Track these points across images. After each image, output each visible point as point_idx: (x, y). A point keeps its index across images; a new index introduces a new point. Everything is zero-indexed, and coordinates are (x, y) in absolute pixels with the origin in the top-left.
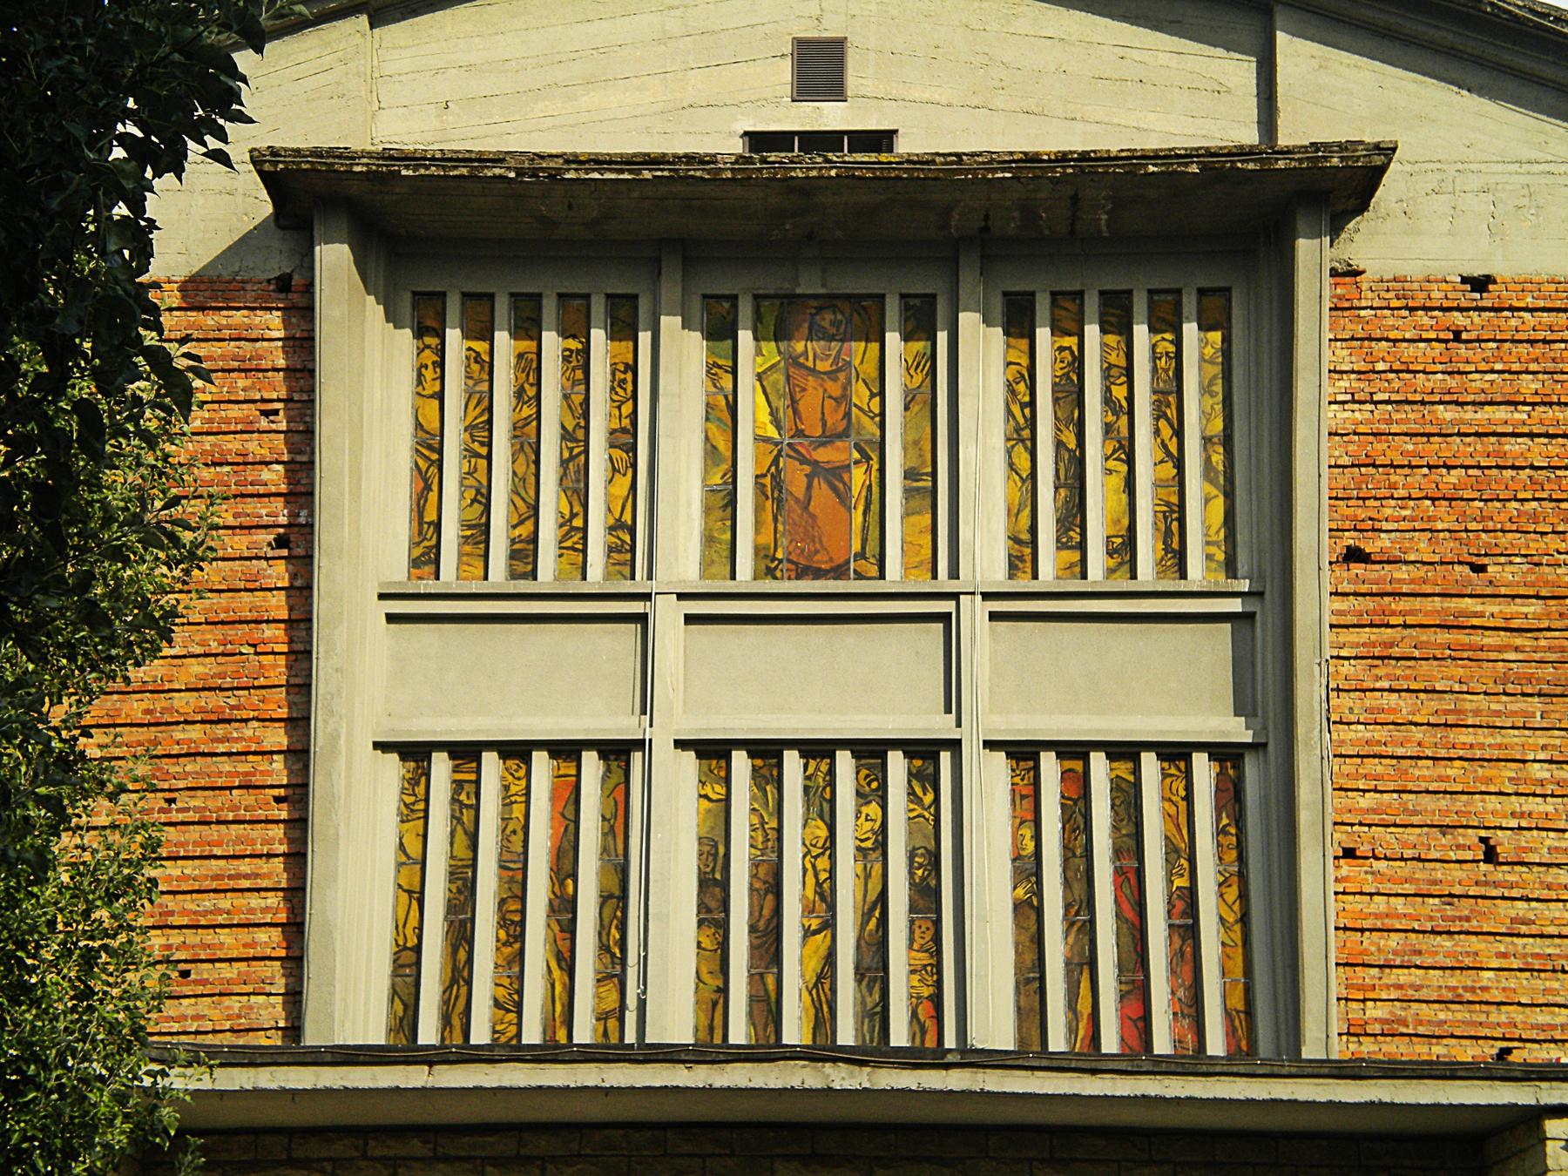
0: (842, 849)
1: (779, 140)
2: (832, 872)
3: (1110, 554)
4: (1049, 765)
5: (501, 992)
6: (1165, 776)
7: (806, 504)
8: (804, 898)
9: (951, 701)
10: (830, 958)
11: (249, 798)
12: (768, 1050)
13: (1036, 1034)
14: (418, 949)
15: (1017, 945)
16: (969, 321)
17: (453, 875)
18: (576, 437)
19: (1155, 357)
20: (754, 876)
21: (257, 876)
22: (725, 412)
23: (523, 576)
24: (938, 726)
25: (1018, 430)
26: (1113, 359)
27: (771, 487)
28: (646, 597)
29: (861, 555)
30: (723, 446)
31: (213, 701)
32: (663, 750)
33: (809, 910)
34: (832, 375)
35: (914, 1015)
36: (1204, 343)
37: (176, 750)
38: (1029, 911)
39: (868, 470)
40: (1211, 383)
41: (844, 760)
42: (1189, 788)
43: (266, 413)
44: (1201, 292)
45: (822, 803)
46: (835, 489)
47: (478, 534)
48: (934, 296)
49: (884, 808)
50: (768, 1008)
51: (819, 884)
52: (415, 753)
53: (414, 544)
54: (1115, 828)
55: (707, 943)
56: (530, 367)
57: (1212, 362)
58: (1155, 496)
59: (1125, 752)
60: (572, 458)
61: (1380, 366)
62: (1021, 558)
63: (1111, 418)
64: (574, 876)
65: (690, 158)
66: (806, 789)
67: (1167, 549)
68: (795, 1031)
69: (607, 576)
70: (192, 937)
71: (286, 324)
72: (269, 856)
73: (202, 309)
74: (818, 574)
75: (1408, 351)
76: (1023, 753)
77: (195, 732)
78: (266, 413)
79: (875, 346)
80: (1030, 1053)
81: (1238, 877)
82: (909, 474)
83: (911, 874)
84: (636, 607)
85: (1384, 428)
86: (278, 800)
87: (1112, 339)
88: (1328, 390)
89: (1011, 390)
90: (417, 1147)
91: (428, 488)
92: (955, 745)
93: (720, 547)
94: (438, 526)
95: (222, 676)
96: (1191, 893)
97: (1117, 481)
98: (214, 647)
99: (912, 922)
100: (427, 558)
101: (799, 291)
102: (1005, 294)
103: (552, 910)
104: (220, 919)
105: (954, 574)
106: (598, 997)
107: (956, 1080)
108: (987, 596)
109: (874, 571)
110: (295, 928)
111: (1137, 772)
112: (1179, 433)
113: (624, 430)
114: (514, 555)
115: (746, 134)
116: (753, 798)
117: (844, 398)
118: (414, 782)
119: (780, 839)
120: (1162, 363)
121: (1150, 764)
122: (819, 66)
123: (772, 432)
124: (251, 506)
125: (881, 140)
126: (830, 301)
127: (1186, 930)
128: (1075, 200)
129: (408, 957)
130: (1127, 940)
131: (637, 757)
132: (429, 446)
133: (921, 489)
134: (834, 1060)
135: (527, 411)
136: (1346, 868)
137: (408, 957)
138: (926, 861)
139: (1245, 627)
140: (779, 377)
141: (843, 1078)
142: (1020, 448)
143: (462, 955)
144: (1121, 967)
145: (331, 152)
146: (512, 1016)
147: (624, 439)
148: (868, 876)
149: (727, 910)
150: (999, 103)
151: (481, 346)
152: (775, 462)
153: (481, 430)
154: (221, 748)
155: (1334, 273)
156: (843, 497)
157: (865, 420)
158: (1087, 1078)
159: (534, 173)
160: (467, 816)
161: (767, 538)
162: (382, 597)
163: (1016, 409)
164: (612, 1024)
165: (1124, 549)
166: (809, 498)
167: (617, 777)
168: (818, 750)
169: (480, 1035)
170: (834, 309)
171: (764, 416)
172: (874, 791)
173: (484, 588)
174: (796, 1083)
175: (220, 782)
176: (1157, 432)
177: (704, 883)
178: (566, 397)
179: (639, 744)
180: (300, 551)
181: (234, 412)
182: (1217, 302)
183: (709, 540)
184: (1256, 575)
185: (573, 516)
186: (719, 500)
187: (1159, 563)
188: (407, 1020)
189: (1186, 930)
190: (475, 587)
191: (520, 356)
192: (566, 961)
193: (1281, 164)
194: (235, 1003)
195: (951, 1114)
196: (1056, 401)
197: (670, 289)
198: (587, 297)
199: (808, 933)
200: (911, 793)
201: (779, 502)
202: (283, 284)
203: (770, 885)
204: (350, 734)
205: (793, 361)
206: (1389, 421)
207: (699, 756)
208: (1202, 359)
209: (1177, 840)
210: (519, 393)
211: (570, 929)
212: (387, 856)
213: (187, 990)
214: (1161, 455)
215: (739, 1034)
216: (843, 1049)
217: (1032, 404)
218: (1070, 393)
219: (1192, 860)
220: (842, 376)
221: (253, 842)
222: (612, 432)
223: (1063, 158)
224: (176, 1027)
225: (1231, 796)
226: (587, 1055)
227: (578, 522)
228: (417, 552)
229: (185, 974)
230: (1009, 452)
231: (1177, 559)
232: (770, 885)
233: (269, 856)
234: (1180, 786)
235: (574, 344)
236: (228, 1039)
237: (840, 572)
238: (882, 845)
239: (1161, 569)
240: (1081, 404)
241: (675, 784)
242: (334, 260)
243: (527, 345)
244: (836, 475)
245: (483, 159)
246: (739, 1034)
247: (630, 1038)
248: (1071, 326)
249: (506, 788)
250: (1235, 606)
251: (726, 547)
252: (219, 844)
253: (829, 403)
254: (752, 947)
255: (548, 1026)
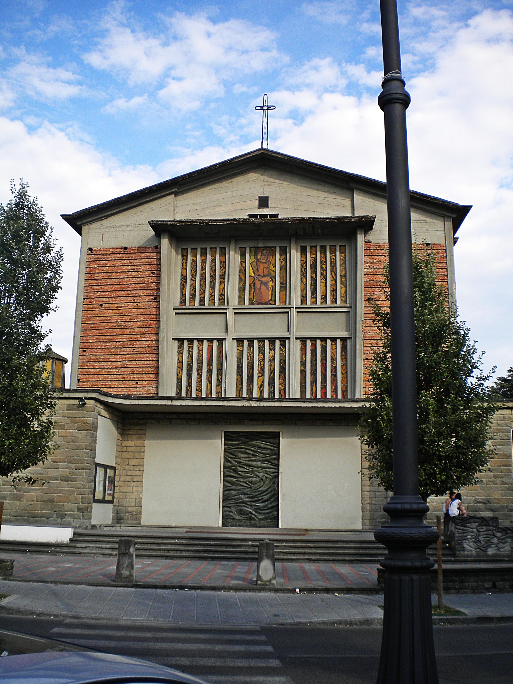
0: (266, 359)
1: (256, 216)
2: (264, 364)
3: (322, 299)
4: (318, 342)
5: (198, 388)
6: (332, 344)
7: (260, 289)
8: (258, 370)
9: (289, 330)
10: (263, 382)
11: (149, 349)
12: (271, 399)
13: (304, 395)
14: (181, 379)
15: (301, 378)
16: (293, 251)
17: (188, 365)
18: (213, 276)
19: (331, 259)
20: (248, 365)
21: (150, 364)
22: (243, 271)
23: (202, 305)
24: (286, 335)
25: (303, 274)
26: (323, 259)
27: (253, 286)
28: (226, 309)
29: (271, 300)
30: (243, 278)
31: (141, 330)
32: (229, 339)
33: (259, 372)
34: (265, 263)
35: (280, 392)
36: (341, 256)
37: (135, 340)
38: (303, 372)
39: (273, 282)
40: (342, 264)
41: (215, 342)
42: (336, 347)
43: (152, 273)
44: (340, 246)
45: (262, 351)
46: (266, 286)
47: (193, 297)
48: (286, 247)
49: (275, 352)
50: (250, 391)
51: (261, 367)
52: (181, 341)
53: (181, 299)
54: (321, 355)
55: (238, 379)
56: (204, 262)
57: (342, 260)
58: (331, 287)
59: (323, 340)
60: (212, 281)
61: (375, 261)
62: (304, 300)
63: (322, 271)
64: (212, 365)
65: (234, 220)
66: (259, 348)
67: (333, 298)
68: (255, 395)
69: (219, 305)
70: (139, 376)
71: (156, 255)
72: (152, 360)
73: (141, 253)
74: (262, 304)
75: (380, 258)
76: (303, 340)
77: (139, 336)
78: (152, 273)
79: (274, 257)
80: (303, 399)
81: (344, 365)
82: (281, 283)
83: (280, 365)
84: (224, 311)
85: (376, 273)
86: (154, 349)
87: (322, 255)
88: (364, 266)
89: (302, 265)
90: (174, 416)
91: (184, 287)
92: (289, 338)
93: (241, 299)
94: (185, 295)
95: (144, 325)
96: (336, 368)
97: (323, 284)
98: (142, 319)
99: (280, 374)
100: (183, 301)
101: (259, 246)
102: (301, 246)
103: (208, 372)
104: (144, 372)
105: (290, 304)
106: (217, 389)
107: (225, 403)
108: (296, 308)
109: (274, 303)
110: (157, 374)
111: (326, 343)
112: (336, 274)
113: (223, 275)
114: (200, 301)
115: (248, 215)
116: (248, 350)
117: (268, 268)
118: (181, 346)
119: (253, 358)
120: (332, 260)
121: (328, 342)
122: (263, 202)
123: (253, 275)
124: (149, 291)
125: (276, 215)
126: (265, 248)
127: (334, 376)
128: (313, 227)
129: (179, 381)
130: (323, 377)
131: (224, 341)
132: (184, 278)
133: (283, 287)
134: (252, 400)
135: (203, 271)
136: (366, 362)
137: (179, 381)
138: (283, 362)
139: (348, 313)
140: (255, 264)
141: (254, 404)
142: (304, 278)
143: (190, 380)
144: (322, 383)
145: (164, 221)
146: (200, 392)
147: (223, 277)
148: (271, 365)
149: (242, 372)
150: (299, 208)
151: (194, 259)
152: (254, 281)
153: (194, 275)
154: (144, 339)
155: (365, 242)
156: (268, 288)
157: (272, 272)
158: (183, 401)
159: (203, 223)
160: (191, 353)
161: (252, 297)
162: (174, 309)
163: (303, 270)
164: (219, 394)
165: (324, 298)
166: (260, 288)
167: (221, 346)
168: (261, 340)
169: (194, 395)
170: (266, 249)
171: (251, 272)
172: (272, 348)
173: (306, 306)
174: (244, 405)
175: (144, 346)
176: (331, 274)
177: (238, 367)
178: (211, 268)
179: (225, 339)
180: (158, 300)
181: (146, 273)
182: (343, 248)
183: (240, 297)
184: (351, 303)
185: (212, 292)
186: (242, 289)
187: (331, 301)
188: (179, 392)
189: (334, 376)
190: (192, 307)
191: (202, 260)
192: (210, 382)
193: (353, 220)
194: (147, 389)
195: (278, 411)
196: (311, 268)
197: (232, 247)
198: (216, 248)
199: (259, 377)
200: (280, 348)
201: (254, 289)
202: (156, 247)
203: (251, 367)
204: (167, 336)
205: (257, 260)
206: (377, 272)
207: (237, 341)
208: (340, 259)
209: (334, 357)
210: (202, 268)
211: (211, 376)
212: (176, 361)
213: (138, 386)
214: (332, 279)
215: (244, 395)
216: (183, 397)
217: (306, 269)
218: (314, 266)
219: (336, 361)
220: (267, 263)
221: (149, 358)
222: (221, 275)
223: (309, 218)
224: (136, 393)
225: (344, 348)
226: (214, 399)
227: (213, 294)
228: (181, 300)
229: (137, 383)
230: (301, 278)
231: (334, 300)
232: (251, 367)
233: (152, 360)
234: (335, 346)
235: (213, 258)
236: (145, 395)
237: (266, 304)
238: (274, 359)
239: (332, 302)
240: (316, 269)
241: (295, 347)
242: (165, 242)
243: (204, 258)
244: (266, 284)
245: (193, 221)
246: (244, 395)
247: (223, 396)
248: (315, 253)
249: (199, 348)
250: (346, 309)
251: (243, 299)
252: (143, 358)
253: (265, 269)
254: (248, 379)
255: (207, 394)
